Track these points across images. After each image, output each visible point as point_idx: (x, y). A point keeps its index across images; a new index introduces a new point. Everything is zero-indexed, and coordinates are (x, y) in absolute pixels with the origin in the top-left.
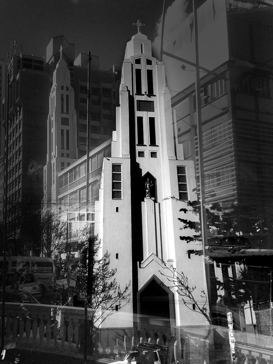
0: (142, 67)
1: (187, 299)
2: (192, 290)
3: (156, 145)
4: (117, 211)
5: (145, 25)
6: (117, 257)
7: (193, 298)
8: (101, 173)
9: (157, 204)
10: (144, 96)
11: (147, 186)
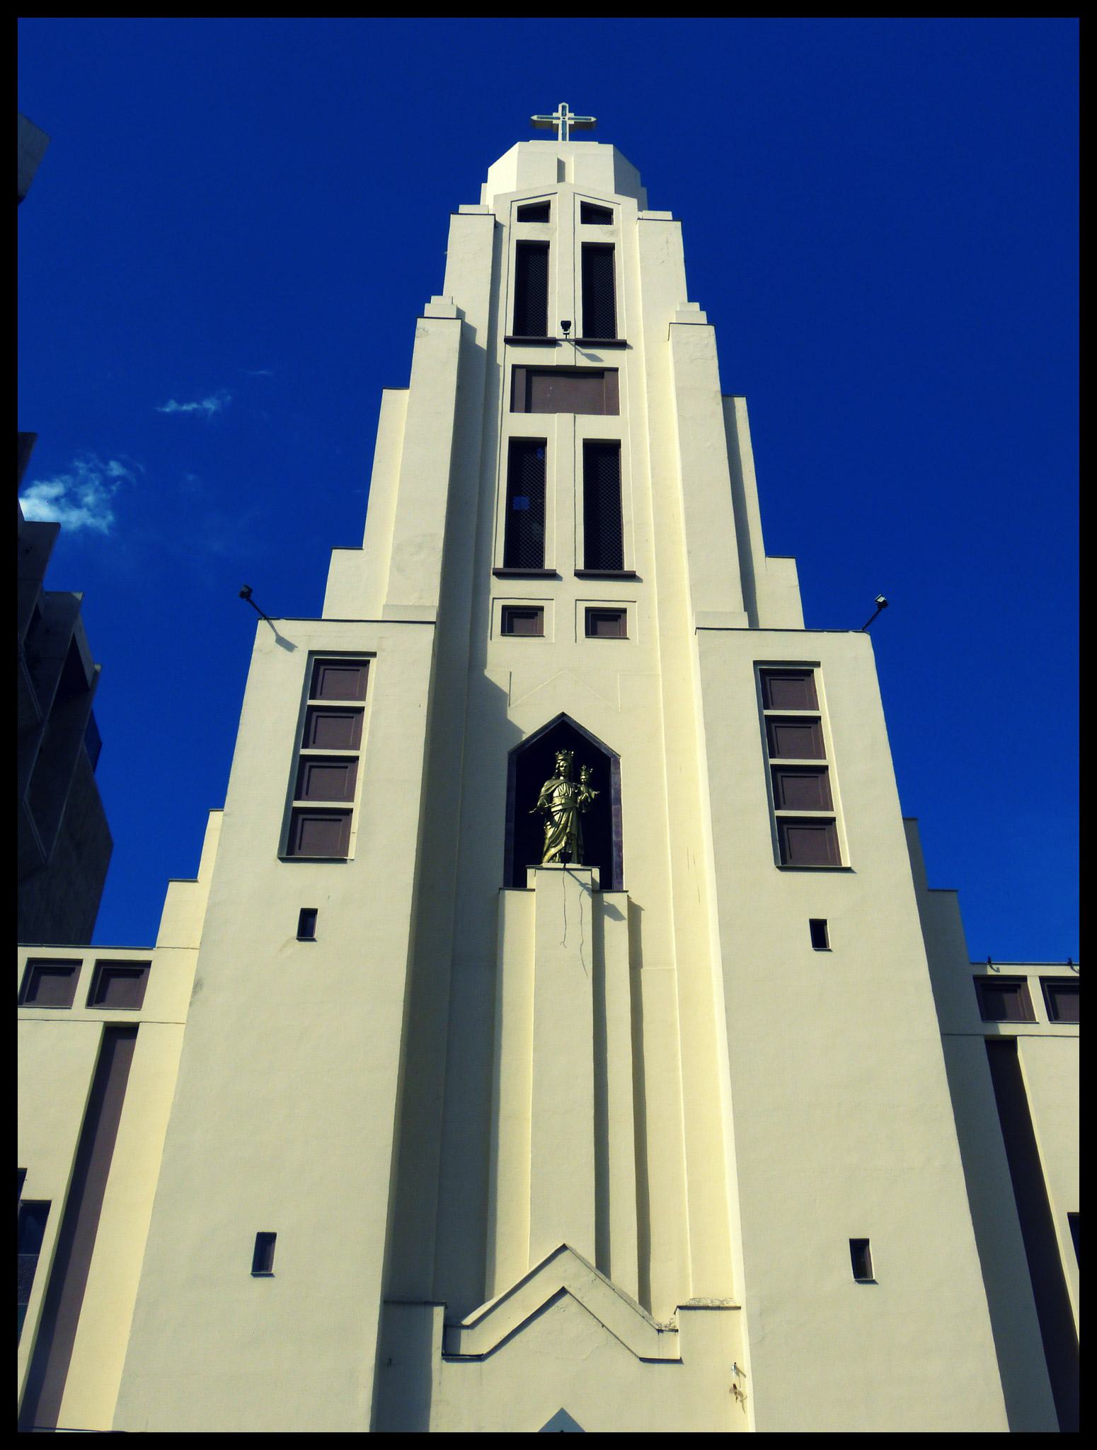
9: (616, 933)
11: (550, 797)
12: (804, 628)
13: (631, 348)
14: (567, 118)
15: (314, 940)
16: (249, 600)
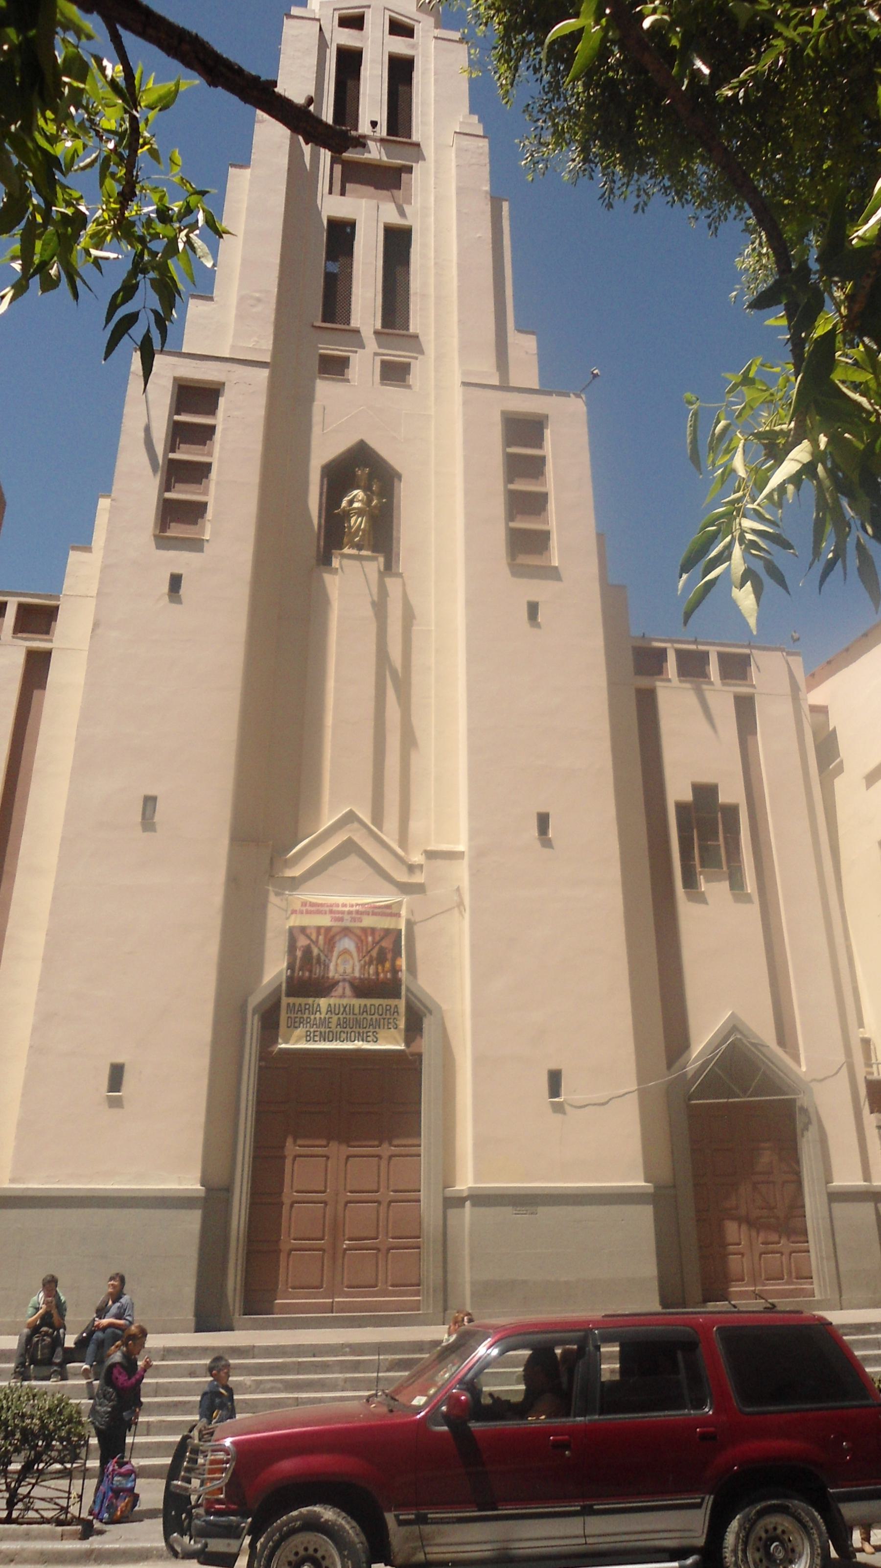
12: (536, 386)
15: (409, 387)
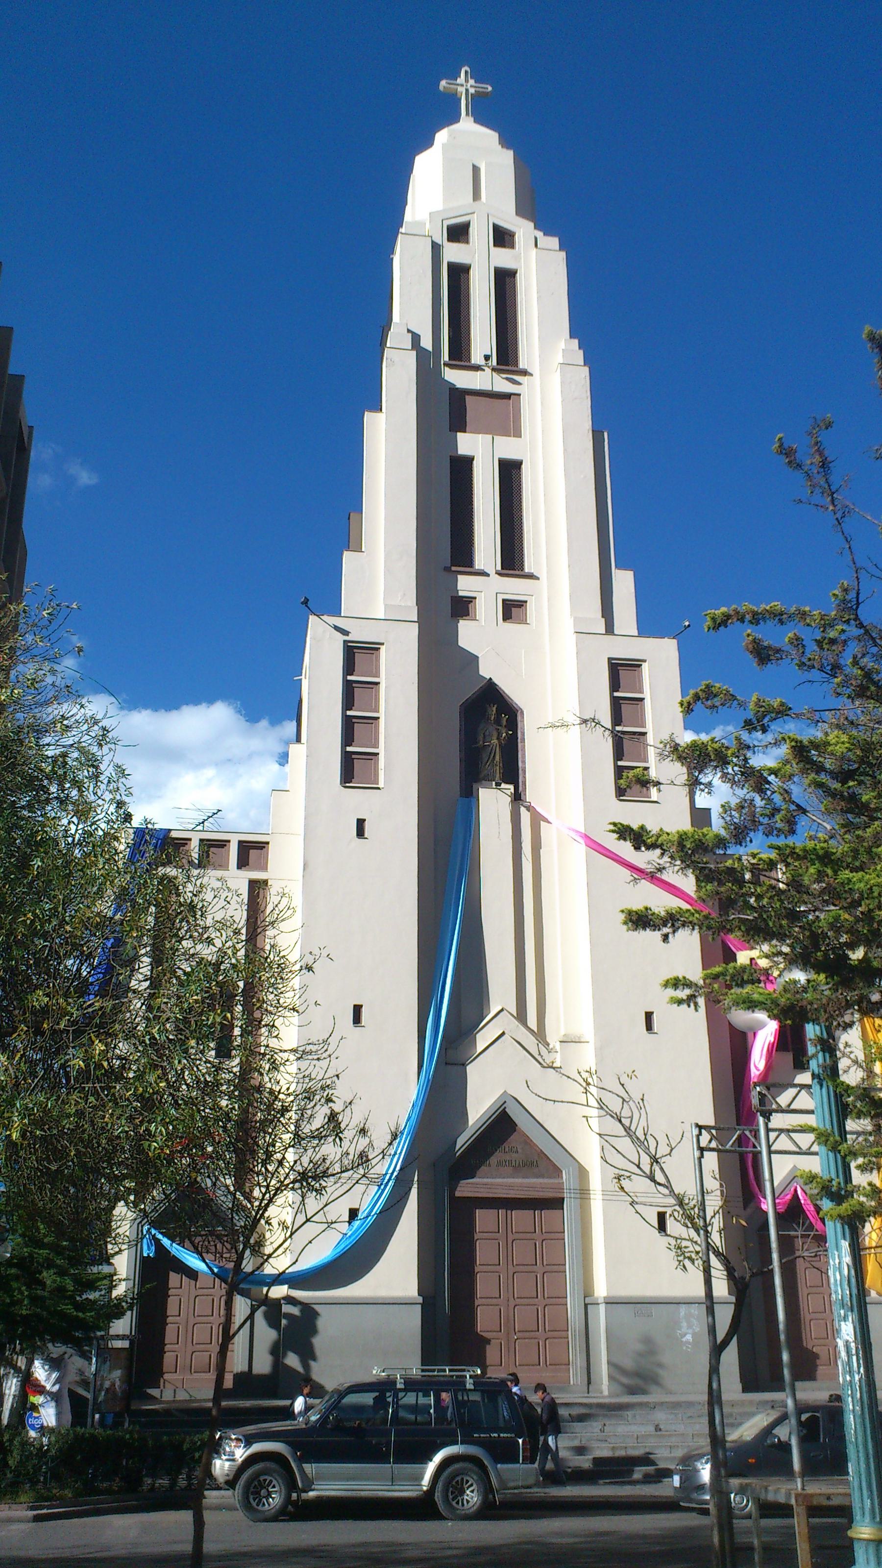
0: (474, 257)
1: (639, 1185)
2: (663, 1150)
3: (526, 570)
4: (360, 832)
5: (490, 89)
6: (357, 1019)
7: (669, 1181)
8: (301, 680)
10: (479, 373)
12: (637, 635)
13: (531, 375)
14: (469, 85)
16: (306, 606)
